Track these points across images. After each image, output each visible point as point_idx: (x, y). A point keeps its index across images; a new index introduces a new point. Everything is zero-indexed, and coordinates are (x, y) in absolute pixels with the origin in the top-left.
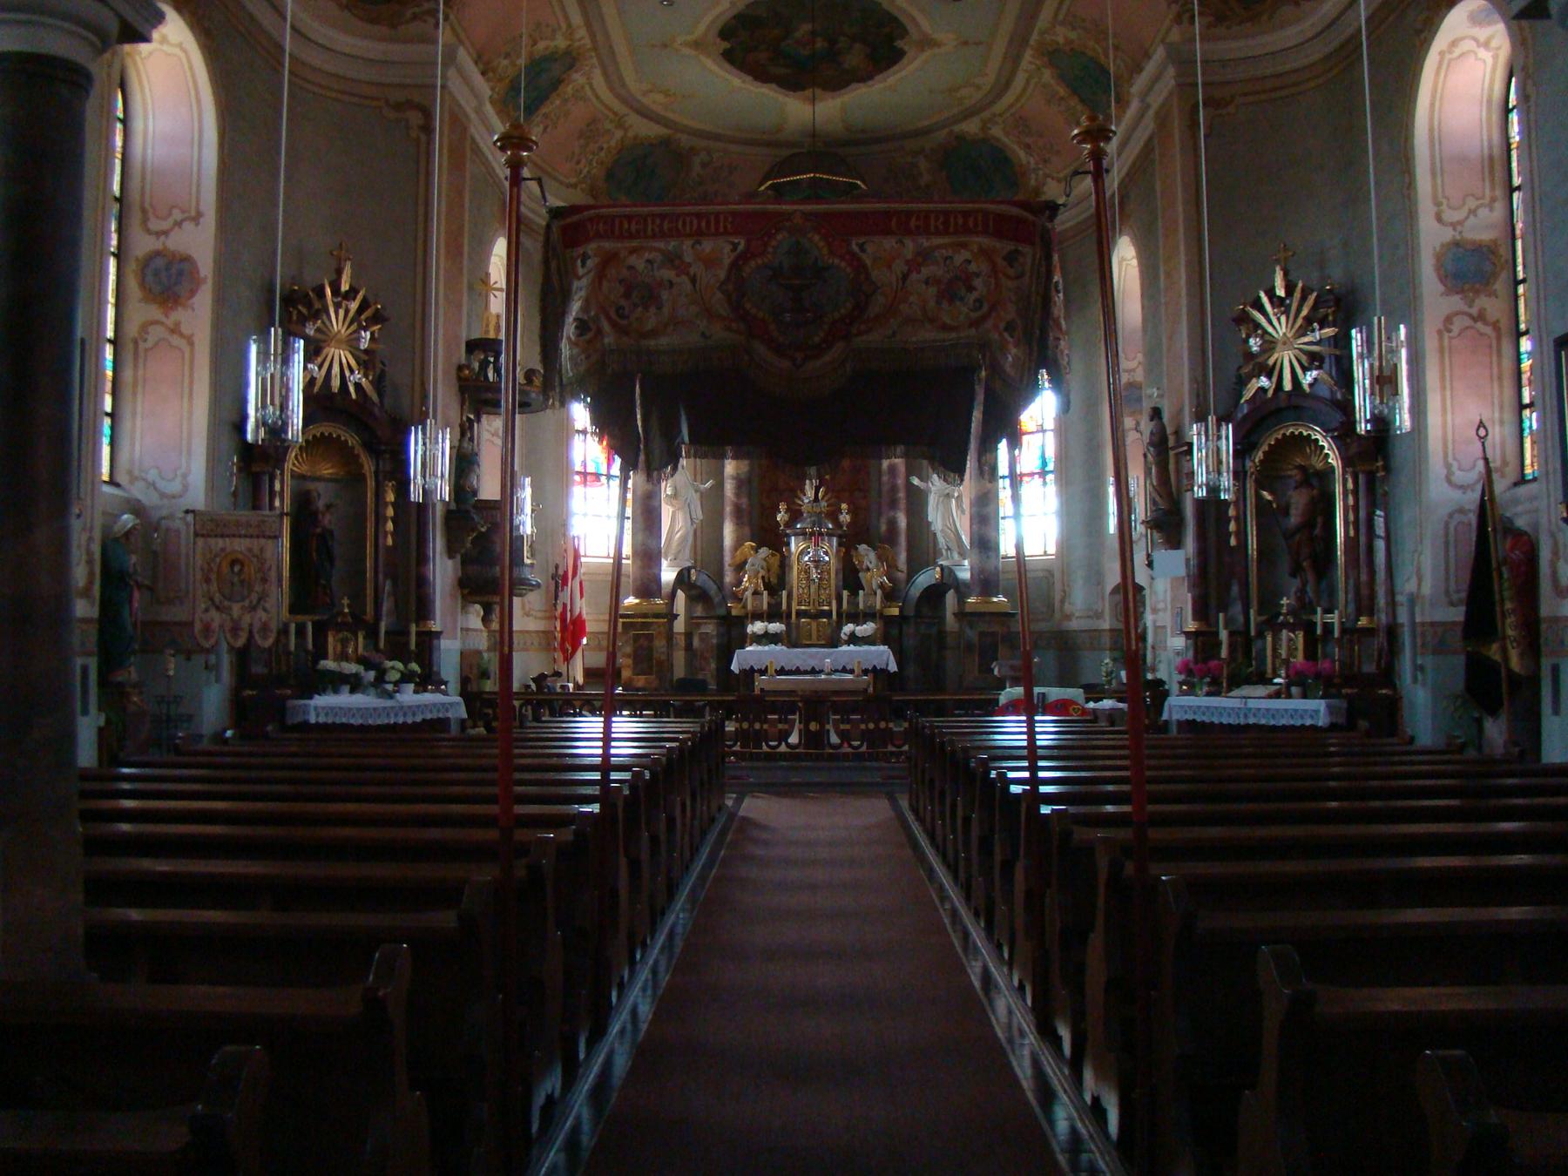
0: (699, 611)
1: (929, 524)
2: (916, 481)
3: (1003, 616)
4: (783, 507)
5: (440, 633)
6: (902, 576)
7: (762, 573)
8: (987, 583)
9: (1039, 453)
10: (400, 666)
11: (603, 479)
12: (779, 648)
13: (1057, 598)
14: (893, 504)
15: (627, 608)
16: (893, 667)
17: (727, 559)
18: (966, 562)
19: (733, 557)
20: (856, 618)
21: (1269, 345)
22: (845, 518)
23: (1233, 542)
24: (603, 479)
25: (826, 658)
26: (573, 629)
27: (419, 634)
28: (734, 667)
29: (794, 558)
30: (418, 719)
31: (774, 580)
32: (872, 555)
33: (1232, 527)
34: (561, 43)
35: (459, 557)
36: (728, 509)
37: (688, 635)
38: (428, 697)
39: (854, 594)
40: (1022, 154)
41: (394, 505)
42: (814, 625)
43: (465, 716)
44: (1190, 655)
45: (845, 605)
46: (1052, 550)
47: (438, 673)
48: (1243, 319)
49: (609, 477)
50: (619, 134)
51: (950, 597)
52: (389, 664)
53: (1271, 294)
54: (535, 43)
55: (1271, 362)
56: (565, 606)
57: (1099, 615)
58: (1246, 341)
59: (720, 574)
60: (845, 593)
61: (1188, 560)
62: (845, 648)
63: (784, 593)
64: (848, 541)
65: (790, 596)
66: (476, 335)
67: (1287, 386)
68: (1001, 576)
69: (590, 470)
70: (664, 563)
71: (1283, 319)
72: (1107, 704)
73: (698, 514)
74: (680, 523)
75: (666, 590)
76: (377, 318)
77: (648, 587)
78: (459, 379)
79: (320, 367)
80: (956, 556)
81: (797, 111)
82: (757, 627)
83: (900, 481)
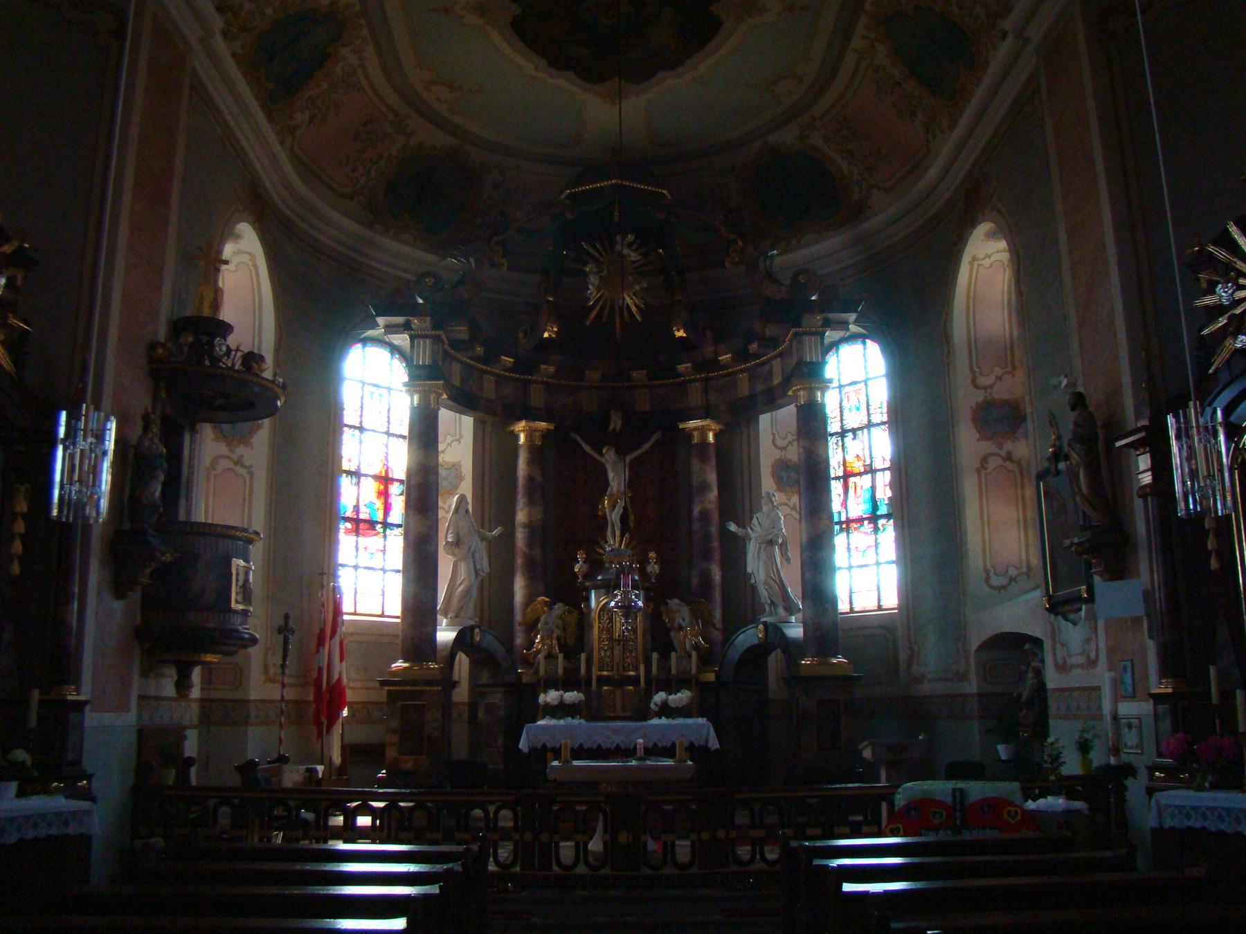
1: (747, 576)
2: (733, 527)
3: (844, 681)
4: (580, 556)
5: (85, 703)
6: (717, 635)
7: (557, 632)
9: (868, 495)
12: (576, 721)
13: (903, 657)
14: (706, 555)
15: (395, 673)
16: (714, 744)
17: (518, 617)
18: (793, 619)
19: (524, 615)
20: (670, 686)
22: (653, 568)
23: (1214, 564)
25: (640, 733)
26: (332, 697)
28: (523, 745)
29: (595, 615)
31: (571, 641)
32: (685, 611)
33: (1211, 544)
35: (136, 597)
36: (519, 561)
37: (473, 705)
38: (38, 803)
39: (665, 656)
40: (845, 167)
42: (618, 692)
44: (1166, 725)
45: (654, 669)
47: (78, 762)
49: (386, 525)
51: (775, 661)
56: (320, 670)
57: (962, 677)
59: (511, 636)
60: (655, 656)
61: (1147, 596)
62: (656, 721)
63: (583, 656)
64: (658, 593)
68: (840, 634)
69: (362, 516)
72: (1055, 803)
73: (485, 565)
74: (462, 575)
80: (781, 611)
81: (603, 114)
82: (551, 696)
83: (714, 529)
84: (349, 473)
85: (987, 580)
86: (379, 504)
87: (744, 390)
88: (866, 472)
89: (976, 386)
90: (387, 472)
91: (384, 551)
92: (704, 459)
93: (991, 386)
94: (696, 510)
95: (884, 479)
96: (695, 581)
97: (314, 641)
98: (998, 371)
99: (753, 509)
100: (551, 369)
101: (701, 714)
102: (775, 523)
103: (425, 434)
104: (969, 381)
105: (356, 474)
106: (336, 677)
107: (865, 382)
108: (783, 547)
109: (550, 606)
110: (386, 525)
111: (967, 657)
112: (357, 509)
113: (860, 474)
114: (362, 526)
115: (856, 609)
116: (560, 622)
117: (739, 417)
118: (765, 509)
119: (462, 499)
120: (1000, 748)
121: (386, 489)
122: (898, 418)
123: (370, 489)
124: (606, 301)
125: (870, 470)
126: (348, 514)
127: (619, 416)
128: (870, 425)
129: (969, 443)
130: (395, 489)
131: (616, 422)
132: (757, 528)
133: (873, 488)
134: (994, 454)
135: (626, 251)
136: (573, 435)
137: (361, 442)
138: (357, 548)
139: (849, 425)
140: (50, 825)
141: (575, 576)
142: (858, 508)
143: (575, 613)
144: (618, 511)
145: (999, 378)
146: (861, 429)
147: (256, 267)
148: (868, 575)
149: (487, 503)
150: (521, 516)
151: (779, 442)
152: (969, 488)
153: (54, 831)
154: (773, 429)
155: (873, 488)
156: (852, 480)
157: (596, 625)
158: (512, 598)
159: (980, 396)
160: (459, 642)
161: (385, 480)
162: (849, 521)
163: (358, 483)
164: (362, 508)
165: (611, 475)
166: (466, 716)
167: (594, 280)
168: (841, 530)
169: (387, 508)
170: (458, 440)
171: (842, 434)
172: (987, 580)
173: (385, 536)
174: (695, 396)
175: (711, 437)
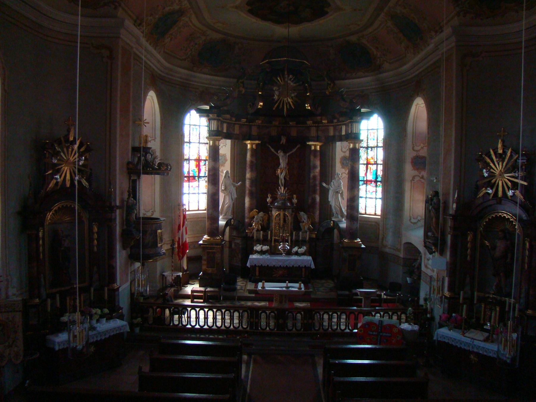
0: (235, 233)
1: (329, 202)
2: (324, 185)
4: (269, 196)
7: (260, 222)
8: (351, 233)
10: (99, 311)
11: (197, 178)
14: (314, 192)
16: (313, 266)
17: (247, 214)
21: (492, 175)
22: (295, 201)
24: (197, 178)
27: (108, 290)
28: (248, 265)
30: (107, 336)
32: (306, 217)
34: (176, 7)
36: (247, 192)
37: (230, 242)
41: (97, 233)
43: (129, 330)
45: (294, 238)
46: (379, 212)
48: (480, 159)
49: (199, 177)
50: (203, 38)
52: (94, 311)
53: (496, 153)
54: (164, 8)
55: (493, 181)
56: (179, 238)
58: (481, 171)
65: (271, 232)
66: (137, 145)
67: (500, 194)
69: (191, 175)
70: (221, 217)
71: (500, 163)
74: (227, 201)
75: (221, 229)
76: (88, 150)
77: (214, 230)
78: (128, 169)
79: (60, 177)
80: (339, 216)
83: (318, 182)
84: (186, 160)
85: (410, 220)
86: (197, 170)
87: (331, 133)
88: (374, 164)
89: (414, 150)
90: (199, 157)
91: (198, 187)
92: (315, 156)
93: (419, 151)
94: (312, 175)
95: (380, 168)
96: (310, 201)
97: (177, 227)
98: (422, 145)
99: (332, 178)
100: (260, 122)
101: (310, 255)
102: (339, 186)
103: (214, 153)
104: (411, 149)
105: (189, 160)
106: (184, 240)
107: (377, 129)
108: (342, 195)
109: (258, 213)
110: (199, 177)
111: (401, 245)
112: (189, 173)
113: (372, 164)
114: (191, 178)
115: (367, 213)
116: (261, 219)
117: (329, 142)
118: (337, 179)
119: (227, 172)
120: (408, 279)
121: (199, 164)
122: (387, 145)
123: (193, 164)
124: (281, 101)
125: (376, 163)
126: (186, 175)
127: (284, 145)
128: (377, 147)
129: (409, 170)
130: (202, 163)
131: (283, 140)
132: (333, 186)
133: (377, 170)
134: (416, 176)
135: (289, 82)
136: (268, 145)
137: (190, 148)
138: (189, 187)
139: (371, 145)
140: (117, 331)
141: (267, 203)
142: (370, 177)
143: (267, 216)
144: (284, 174)
145: (422, 148)
146: (374, 147)
147: (153, 100)
148: (371, 202)
149: (236, 169)
150: (248, 175)
151: (344, 150)
152: (407, 186)
153: (118, 332)
154: (341, 149)
155: (377, 170)
156: (369, 166)
157: (274, 221)
158: (244, 204)
159: (414, 154)
160: (227, 225)
161: (198, 160)
162: (367, 181)
163: (189, 163)
164: (191, 172)
165: (281, 161)
166: (228, 245)
167: (277, 93)
168: (364, 183)
169: (199, 171)
170: (225, 146)
171: (367, 148)
172: (410, 220)
173: (199, 181)
174: (313, 132)
175: (318, 148)
